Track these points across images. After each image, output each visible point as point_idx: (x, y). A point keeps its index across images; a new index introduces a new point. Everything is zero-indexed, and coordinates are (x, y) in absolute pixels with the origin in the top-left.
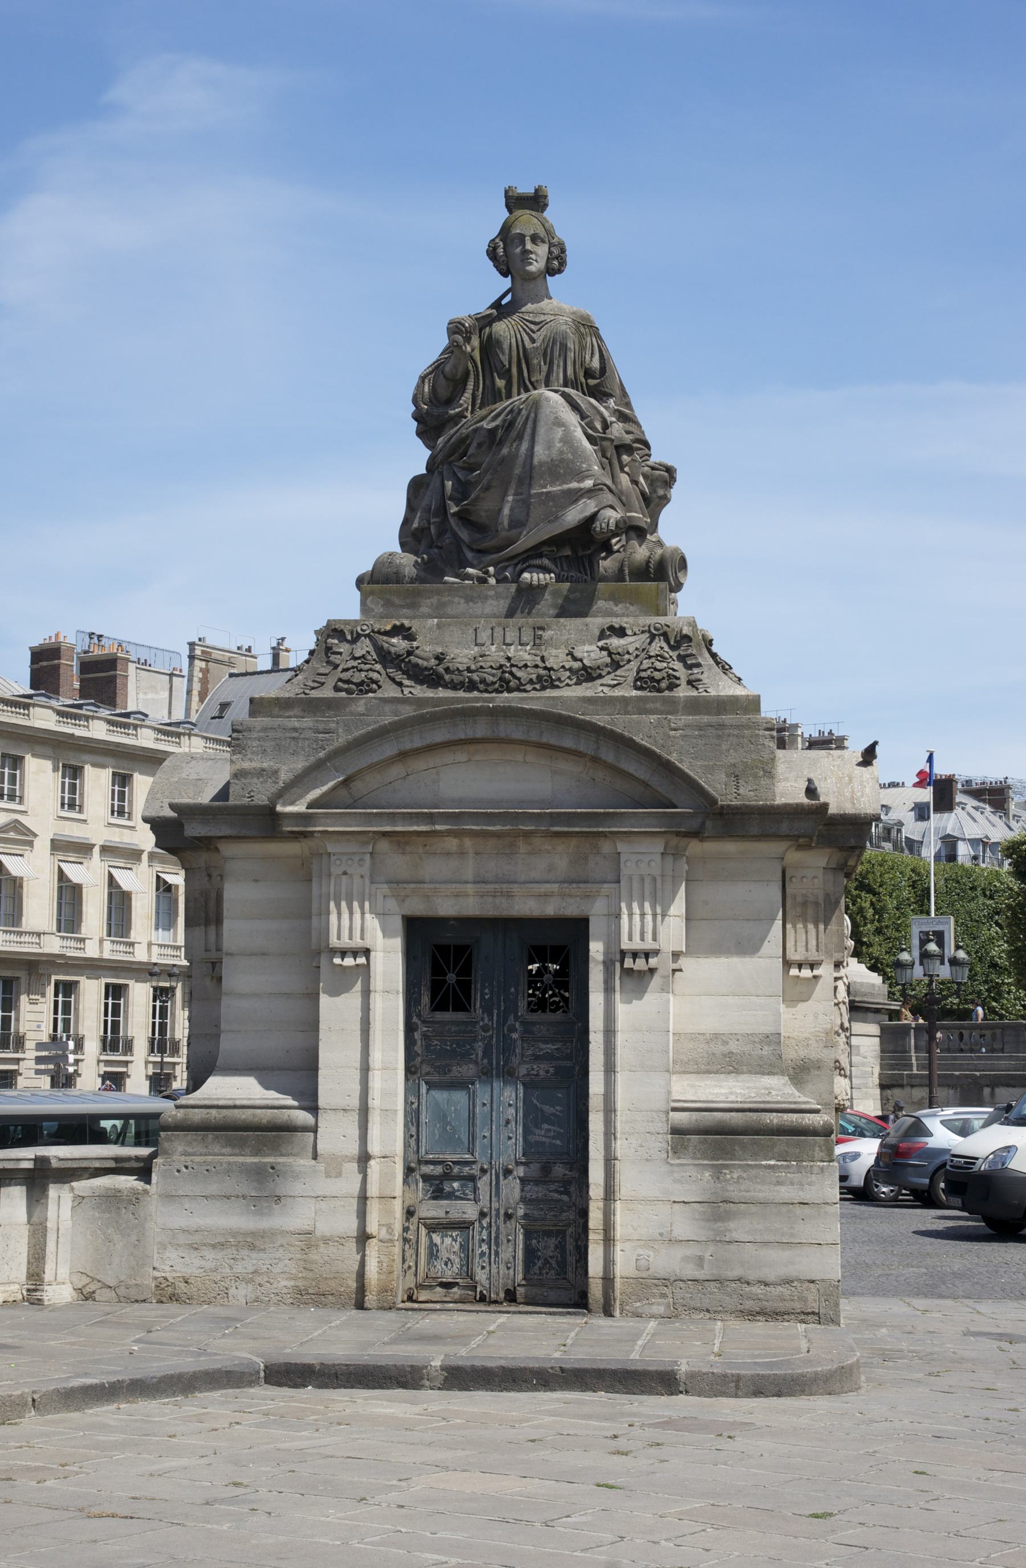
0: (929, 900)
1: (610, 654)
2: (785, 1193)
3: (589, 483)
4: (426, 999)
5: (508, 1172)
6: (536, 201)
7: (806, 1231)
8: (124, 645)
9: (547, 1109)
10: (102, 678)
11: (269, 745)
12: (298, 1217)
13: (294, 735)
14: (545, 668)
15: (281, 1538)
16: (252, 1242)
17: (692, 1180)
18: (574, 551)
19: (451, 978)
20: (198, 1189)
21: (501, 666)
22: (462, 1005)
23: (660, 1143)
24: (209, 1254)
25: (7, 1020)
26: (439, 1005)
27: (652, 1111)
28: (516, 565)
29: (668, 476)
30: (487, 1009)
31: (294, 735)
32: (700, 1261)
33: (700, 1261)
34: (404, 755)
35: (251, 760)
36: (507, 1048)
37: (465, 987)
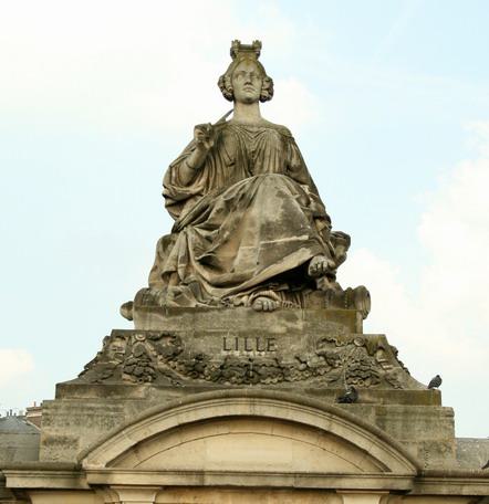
1: (326, 358)
3: (305, 237)
6: (255, 49)
8: (167, 266)
11: (71, 419)
13: (91, 412)
14: (279, 367)
18: (291, 288)
21: (246, 365)
28: (249, 295)
29: (345, 240)
31: (91, 412)
34: (136, 448)
35: (57, 431)
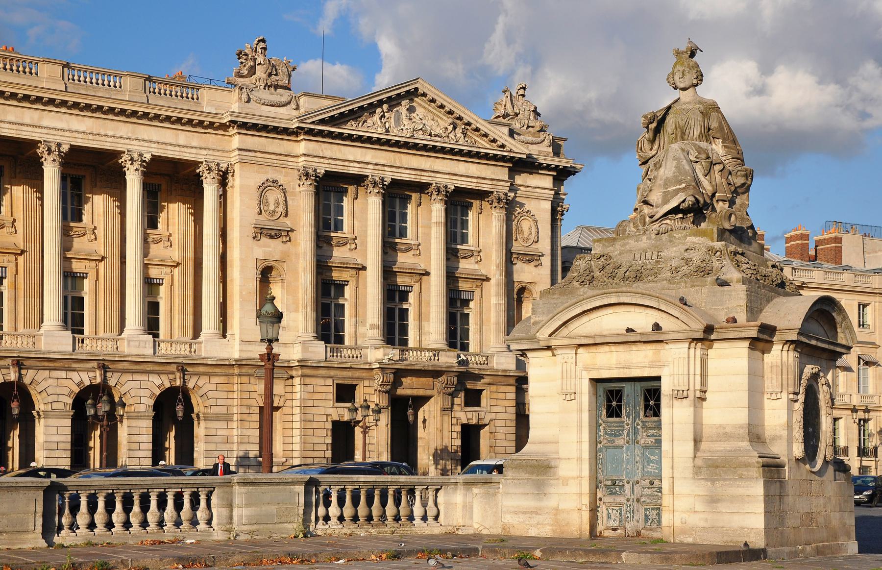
2: (741, 491)
4: (604, 413)
5: (638, 482)
9: (652, 457)
10: (734, 320)
12: (551, 502)
16: (536, 512)
17: (701, 488)
19: (614, 403)
23: (689, 473)
24: (521, 516)
26: (610, 415)
27: (695, 457)
30: (628, 416)
36: (636, 433)
37: (620, 407)
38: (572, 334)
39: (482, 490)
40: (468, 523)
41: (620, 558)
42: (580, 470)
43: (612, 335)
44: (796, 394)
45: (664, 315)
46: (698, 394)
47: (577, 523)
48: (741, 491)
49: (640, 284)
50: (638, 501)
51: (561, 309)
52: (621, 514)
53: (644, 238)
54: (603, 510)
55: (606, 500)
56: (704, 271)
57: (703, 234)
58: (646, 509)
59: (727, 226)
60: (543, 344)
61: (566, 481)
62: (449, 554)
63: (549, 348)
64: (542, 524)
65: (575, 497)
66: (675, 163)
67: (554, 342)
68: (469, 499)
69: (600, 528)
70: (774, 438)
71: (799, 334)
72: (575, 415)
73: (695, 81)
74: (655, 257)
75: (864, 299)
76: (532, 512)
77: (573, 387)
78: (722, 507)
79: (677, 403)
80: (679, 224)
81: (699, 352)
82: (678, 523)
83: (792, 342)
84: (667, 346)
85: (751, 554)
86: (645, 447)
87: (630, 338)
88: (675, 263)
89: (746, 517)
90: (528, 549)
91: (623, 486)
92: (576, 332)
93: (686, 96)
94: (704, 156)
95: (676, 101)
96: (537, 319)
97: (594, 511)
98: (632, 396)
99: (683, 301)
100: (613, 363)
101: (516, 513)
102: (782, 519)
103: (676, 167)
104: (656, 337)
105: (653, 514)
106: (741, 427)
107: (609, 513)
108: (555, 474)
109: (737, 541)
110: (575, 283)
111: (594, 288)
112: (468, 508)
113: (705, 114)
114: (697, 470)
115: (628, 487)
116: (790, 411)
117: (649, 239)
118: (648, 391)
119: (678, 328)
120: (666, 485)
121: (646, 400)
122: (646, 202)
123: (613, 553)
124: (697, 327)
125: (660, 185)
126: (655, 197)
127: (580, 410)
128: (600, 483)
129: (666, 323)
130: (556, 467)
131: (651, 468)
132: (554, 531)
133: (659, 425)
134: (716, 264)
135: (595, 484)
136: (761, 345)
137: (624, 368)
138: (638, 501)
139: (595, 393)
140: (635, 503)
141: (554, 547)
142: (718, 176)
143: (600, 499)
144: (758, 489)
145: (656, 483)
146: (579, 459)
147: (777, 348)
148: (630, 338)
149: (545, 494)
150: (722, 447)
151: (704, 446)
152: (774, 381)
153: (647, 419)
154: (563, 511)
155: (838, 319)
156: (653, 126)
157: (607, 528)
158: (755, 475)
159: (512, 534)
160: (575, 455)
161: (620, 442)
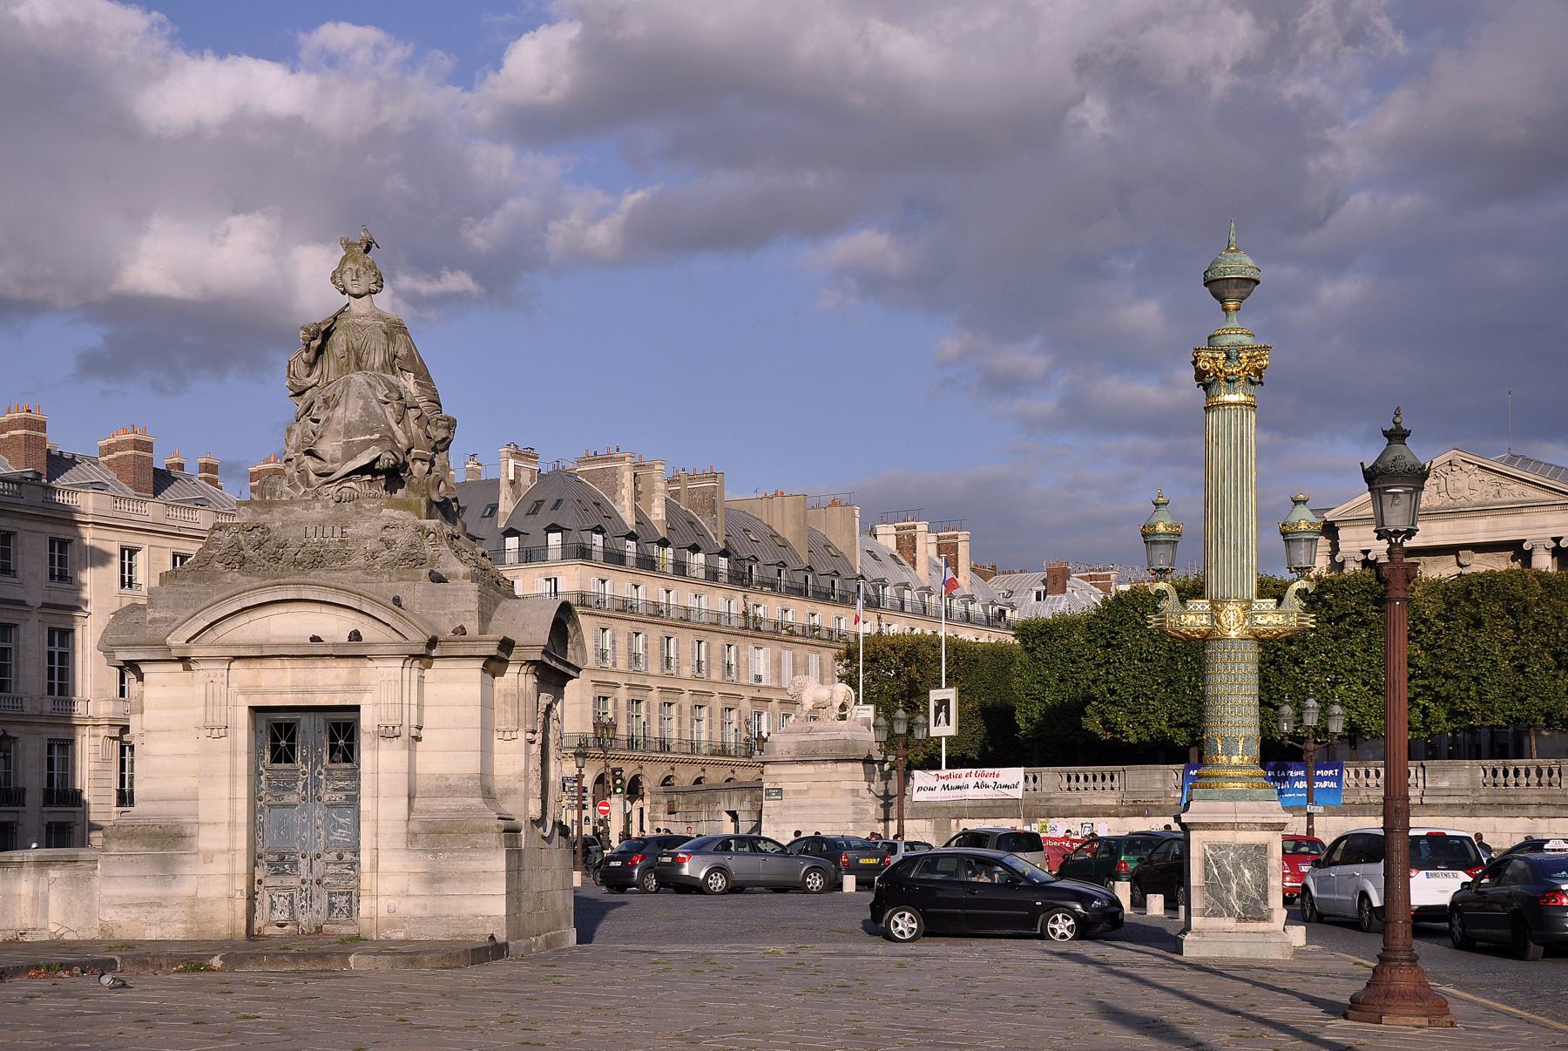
0: (1501, 1001)
2: (474, 865)
4: (268, 756)
5: (319, 856)
7: (486, 888)
9: (342, 820)
10: (463, 631)
12: (186, 888)
15: (897, 627)
16: (158, 904)
17: (419, 863)
19: (283, 743)
20: (127, 872)
22: (289, 760)
23: (400, 842)
24: (134, 910)
25: (7, 775)
26: (276, 759)
30: (305, 761)
32: (425, 907)
33: (425, 907)
36: (317, 785)
37: (292, 748)
38: (221, 641)
39: (65, 873)
40: (40, 923)
41: (347, 963)
42: (233, 840)
43: (292, 645)
44: (534, 732)
45: (366, 619)
46: (414, 732)
47: (227, 917)
48: (474, 865)
49: (322, 573)
50: (319, 882)
51: (208, 603)
52: (291, 903)
53: (318, 505)
54: (264, 898)
55: (269, 882)
56: (413, 559)
57: (404, 505)
58: (330, 894)
59: (435, 497)
60: (175, 653)
61: (209, 857)
62: (77, 970)
63: (183, 660)
64: (168, 921)
65: (224, 879)
66: (361, 402)
67: (195, 652)
68: (42, 887)
69: (258, 924)
70: (508, 792)
71: (544, 652)
72: (225, 760)
73: (373, 287)
74: (337, 534)
75: (131, 540)
76: (151, 904)
77: (223, 719)
78: (447, 888)
79: (383, 744)
80: (366, 490)
81: (415, 673)
82: (383, 913)
83: (533, 663)
84: (370, 664)
85: (493, 951)
86: (331, 806)
87: (314, 651)
88: (370, 545)
89: (481, 901)
90: (199, 957)
91: (296, 862)
92: (228, 638)
93: (360, 307)
94: (395, 396)
95: (342, 311)
96: (157, 615)
97: (251, 898)
98: (312, 734)
99: (397, 601)
100: (285, 685)
101: (124, 906)
102: (519, 908)
103: (364, 409)
104: (354, 650)
105: (341, 901)
106: (471, 778)
107: (272, 902)
108: (191, 846)
109: (480, 934)
110: (217, 565)
111: (249, 573)
112: (40, 902)
113: (390, 336)
114: (412, 838)
115: (303, 864)
116: (527, 754)
117: (326, 506)
118: (336, 725)
119: (386, 639)
120: (365, 858)
121: (333, 738)
122: (310, 453)
123: (336, 957)
124: (417, 639)
125: (338, 432)
126: (329, 447)
127: (233, 753)
128: (260, 857)
129: (369, 631)
130: (192, 836)
131: (339, 835)
132: (187, 930)
133: (355, 775)
134: (429, 551)
135: (254, 859)
136: (493, 665)
137: (304, 692)
138: (319, 882)
139: (254, 727)
140: (315, 887)
141: (189, 958)
142: (413, 426)
143: (260, 882)
144: (499, 862)
145: (348, 856)
146: (232, 824)
147: (512, 670)
148: (314, 651)
149: (175, 877)
150: (444, 806)
151: (417, 803)
152: (509, 716)
153: (334, 766)
154: (203, 900)
155: (571, 630)
156: (317, 342)
157: (270, 923)
158: (494, 843)
159: (117, 937)
160: (225, 817)
161: (293, 799)
